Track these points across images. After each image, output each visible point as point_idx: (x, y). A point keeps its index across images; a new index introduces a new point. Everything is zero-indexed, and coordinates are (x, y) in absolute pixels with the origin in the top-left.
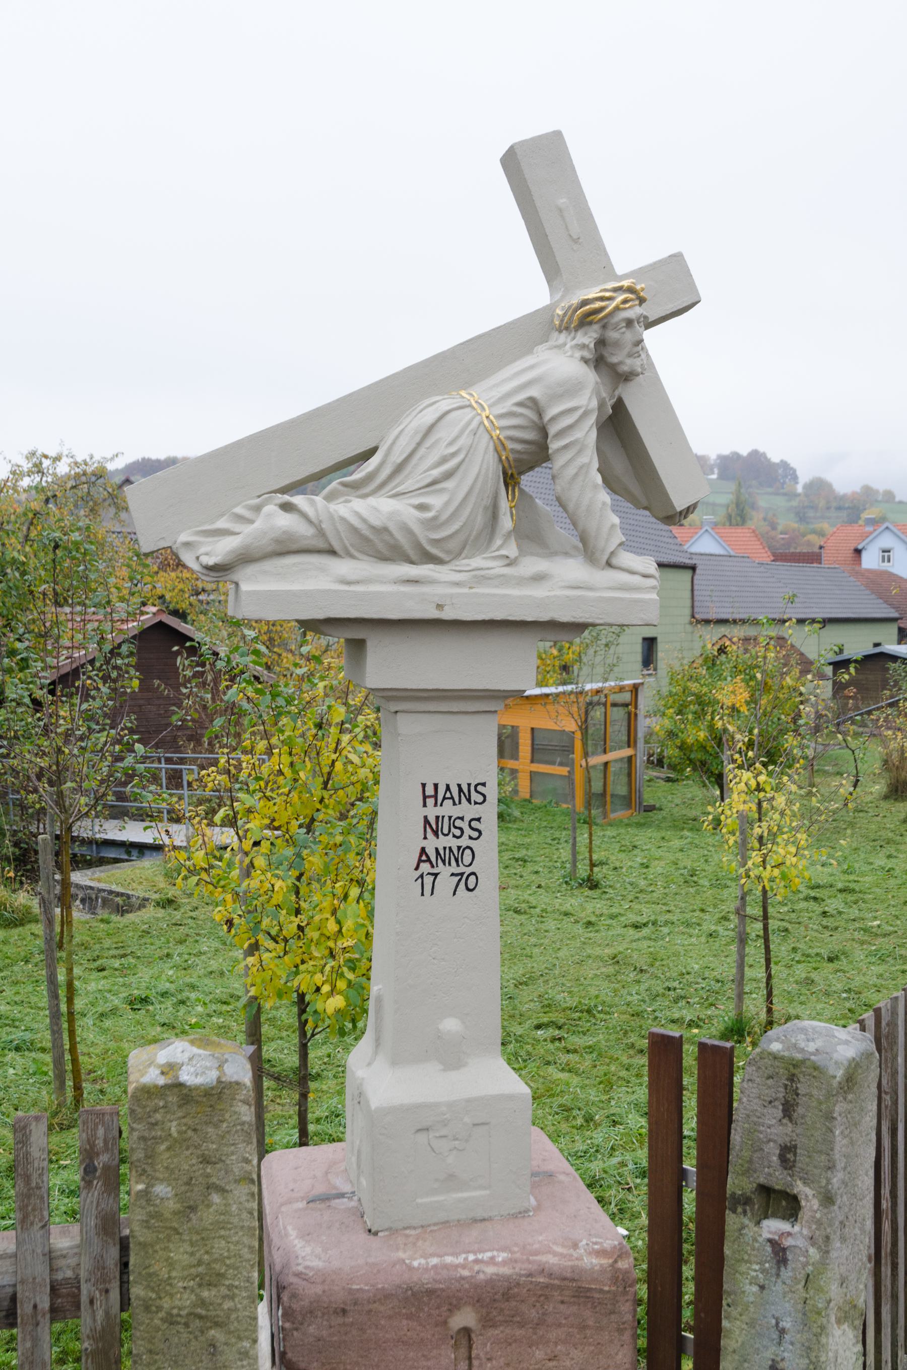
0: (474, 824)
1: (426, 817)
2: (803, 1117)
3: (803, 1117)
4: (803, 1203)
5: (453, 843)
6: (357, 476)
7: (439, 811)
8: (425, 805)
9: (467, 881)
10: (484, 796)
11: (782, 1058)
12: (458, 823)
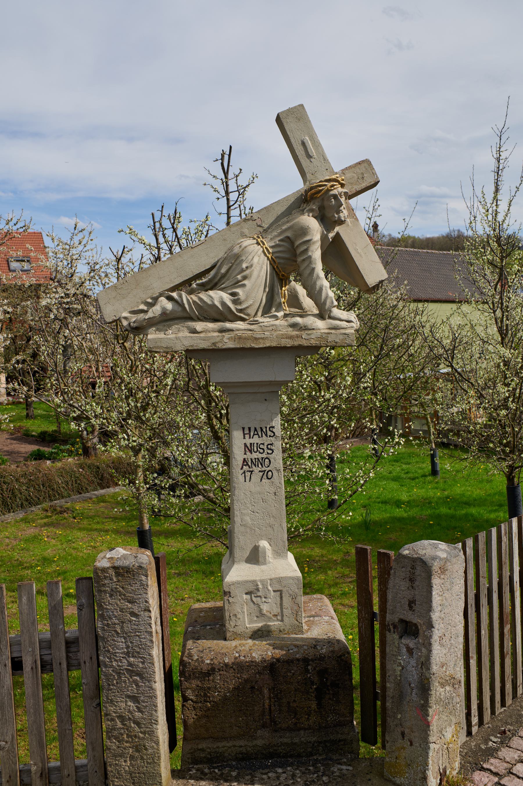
0: (269, 446)
1: (245, 444)
2: (418, 586)
3: (418, 586)
4: (419, 627)
5: (260, 456)
6: (204, 280)
7: (252, 441)
8: (244, 438)
9: (266, 475)
10: (274, 433)
11: (409, 557)
12: (262, 446)
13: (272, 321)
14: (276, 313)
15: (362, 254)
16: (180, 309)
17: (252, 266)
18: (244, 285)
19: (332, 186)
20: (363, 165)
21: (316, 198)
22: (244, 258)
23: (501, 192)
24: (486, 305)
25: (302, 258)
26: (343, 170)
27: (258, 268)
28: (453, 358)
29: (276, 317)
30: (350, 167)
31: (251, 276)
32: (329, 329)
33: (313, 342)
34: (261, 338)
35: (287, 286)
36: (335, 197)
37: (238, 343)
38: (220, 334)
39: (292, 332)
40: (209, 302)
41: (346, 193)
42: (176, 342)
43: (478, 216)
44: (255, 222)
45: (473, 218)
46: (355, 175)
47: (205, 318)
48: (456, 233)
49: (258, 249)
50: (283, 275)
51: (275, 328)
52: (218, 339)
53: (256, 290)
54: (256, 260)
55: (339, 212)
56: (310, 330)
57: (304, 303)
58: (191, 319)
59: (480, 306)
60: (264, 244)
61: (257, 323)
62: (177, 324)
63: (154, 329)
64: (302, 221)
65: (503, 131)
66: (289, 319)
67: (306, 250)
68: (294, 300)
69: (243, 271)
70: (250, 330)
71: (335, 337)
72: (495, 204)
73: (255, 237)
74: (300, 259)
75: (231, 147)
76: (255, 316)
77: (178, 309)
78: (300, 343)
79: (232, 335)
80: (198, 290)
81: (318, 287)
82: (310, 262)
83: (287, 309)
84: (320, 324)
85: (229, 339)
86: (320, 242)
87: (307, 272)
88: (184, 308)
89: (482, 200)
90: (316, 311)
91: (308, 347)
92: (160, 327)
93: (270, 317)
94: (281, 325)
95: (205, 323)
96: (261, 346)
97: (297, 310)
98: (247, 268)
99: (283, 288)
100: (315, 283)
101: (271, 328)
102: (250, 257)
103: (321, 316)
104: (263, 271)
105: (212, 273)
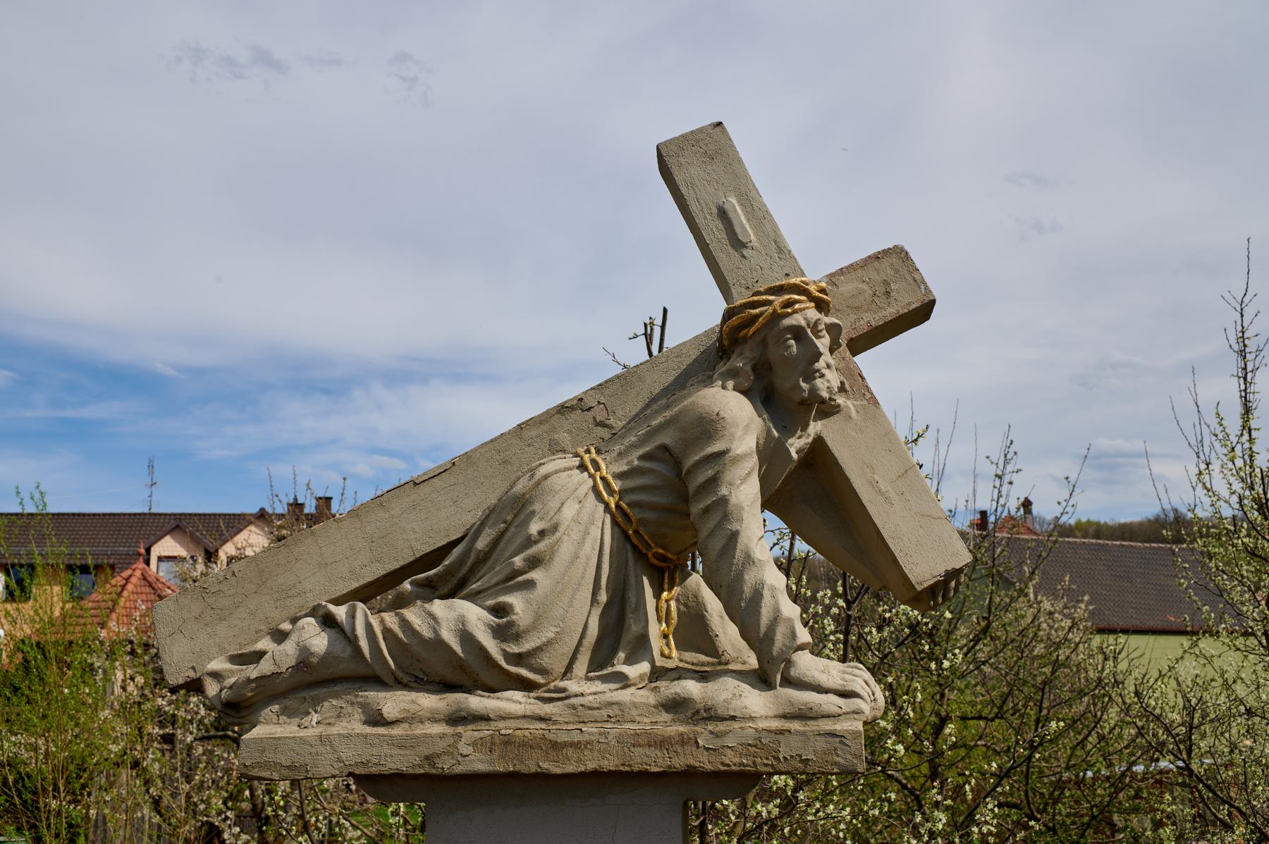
13: (610, 692)
14: (626, 669)
15: (892, 494)
16: (349, 651)
17: (555, 528)
18: (530, 584)
19: (789, 304)
20: (886, 262)
21: (745, 339)
22: (537, 507)
23: (1256, 413)
24: (1252, 639)
25: (702, 505)
26: (831, 275)
27: (575, 536)
28: (1189, 752)
29: (622, 680)
30: (852, 268)
31: (551, 559)
32: (785, 717)
33: (732, 760)
34: (572, 745)
35: (676, 590)
36: (798, 333)
37: (501, 757)
38: (449, 730)
39: (674, 728)
40: (427, 633)
41: (834, 330)
42: (320, 749)
43: (1213, 459)
44: (589, 415)
45: (1203, 466)
46: (865, 286)
47: (418, 680)
48: (1171, 516)
49: (583, 482)
50: (663, 558)
51: (618, 712)
52: (441, 745)
53: (566, 600)
54: (569, 512)
55: (811, 375)
56: (723, 719)
57: (721, 636)
58: (376, 680)
59: (1240, 642)
60: (597, 468)
61: (562, 695)
62: (337, 697)
63: (276, 708)
64: (702, 402)
65: (1246, 300)
66: (662, 684)
67: (714, 482)
68: (693, 630)
69: (530, 542)
70: (541, 719)
71: (802, 744)
72: (1246, 437)
73: (581, 450)
74: (696, 508)
75: (665, 311)
76: (565, 674)
77: (345, 652)
78: (692, 762)
79: (485, 731)
80: (418, 597)
81: (747, 590)
82: (726, 517)
83: (675, 653)
84: (756, 703)
85: (474, 744)
86: (755, 459)
87: (717, 544)
88: (358, 650)
89: (1219, 429)
90: (753, 662)
91: (716, 774)
92: (291, 702)
93: (605, 679)
94: (634, 705)
95: (413, 695)
96: (571, 768)
97: (703, 658)
98: (542, 533)
99: (665, 594)
100: (739, 577)
101: (604, 713)
102: (553, 504)
103: (762, 679)
104: (589, 541)
105: (457, 551)
